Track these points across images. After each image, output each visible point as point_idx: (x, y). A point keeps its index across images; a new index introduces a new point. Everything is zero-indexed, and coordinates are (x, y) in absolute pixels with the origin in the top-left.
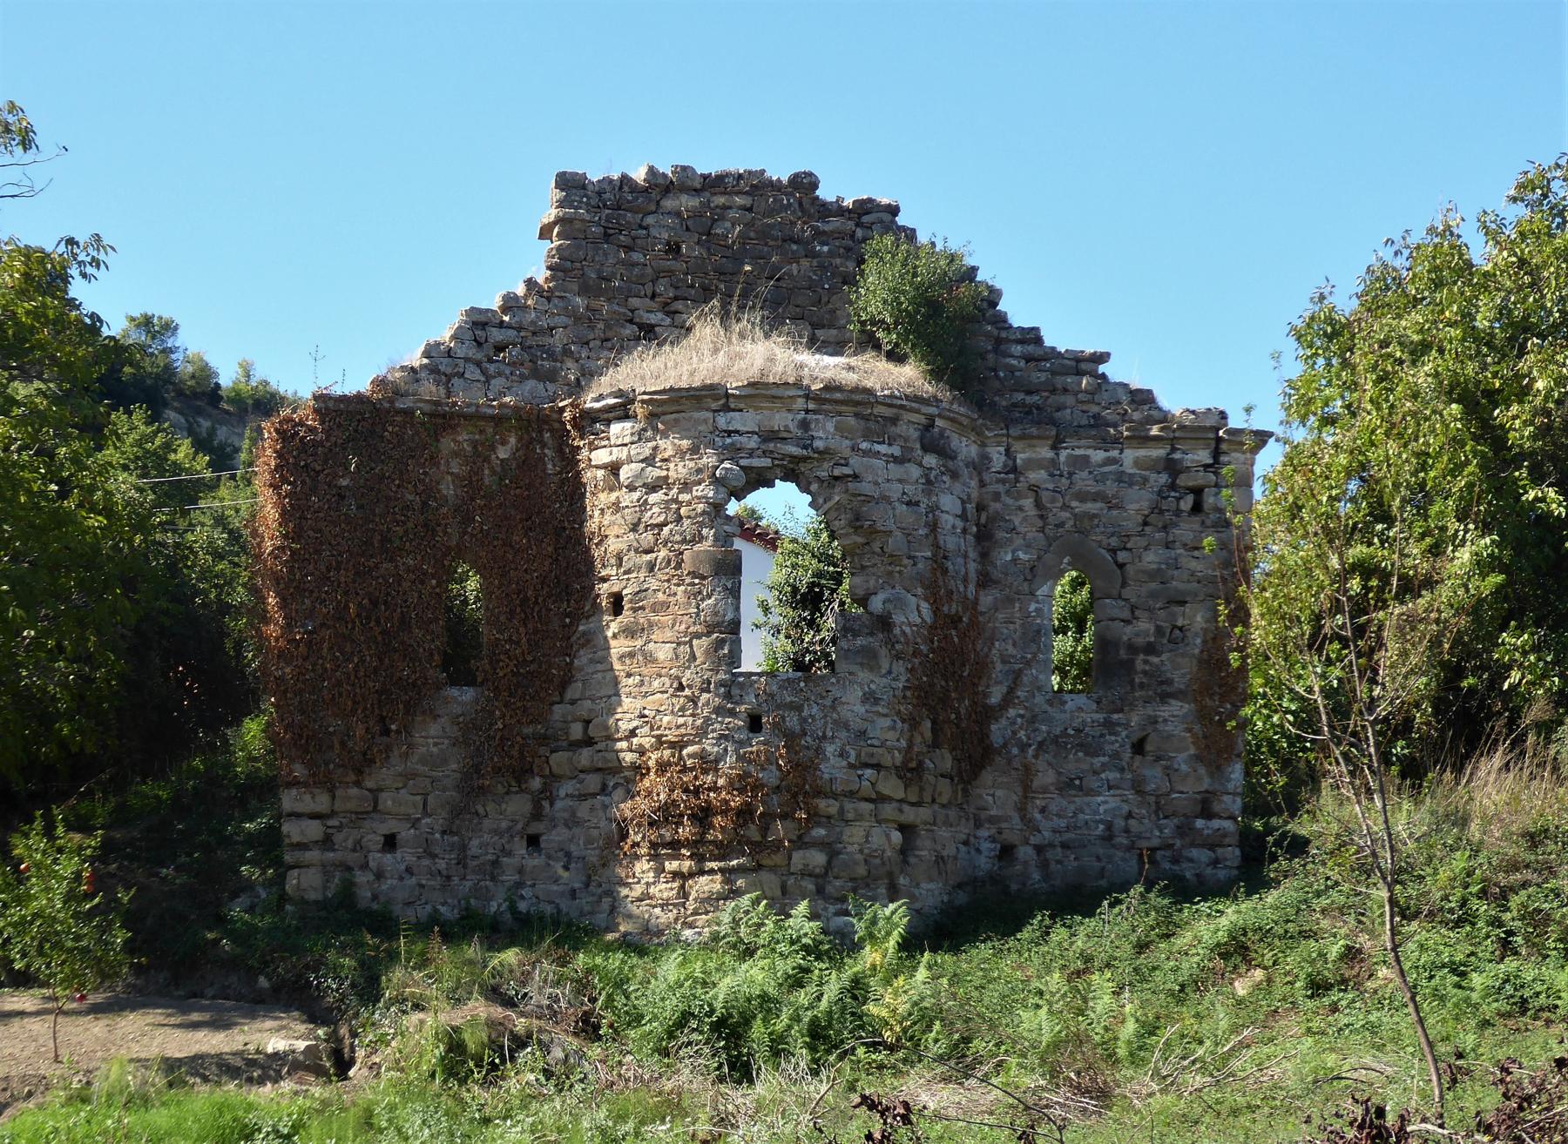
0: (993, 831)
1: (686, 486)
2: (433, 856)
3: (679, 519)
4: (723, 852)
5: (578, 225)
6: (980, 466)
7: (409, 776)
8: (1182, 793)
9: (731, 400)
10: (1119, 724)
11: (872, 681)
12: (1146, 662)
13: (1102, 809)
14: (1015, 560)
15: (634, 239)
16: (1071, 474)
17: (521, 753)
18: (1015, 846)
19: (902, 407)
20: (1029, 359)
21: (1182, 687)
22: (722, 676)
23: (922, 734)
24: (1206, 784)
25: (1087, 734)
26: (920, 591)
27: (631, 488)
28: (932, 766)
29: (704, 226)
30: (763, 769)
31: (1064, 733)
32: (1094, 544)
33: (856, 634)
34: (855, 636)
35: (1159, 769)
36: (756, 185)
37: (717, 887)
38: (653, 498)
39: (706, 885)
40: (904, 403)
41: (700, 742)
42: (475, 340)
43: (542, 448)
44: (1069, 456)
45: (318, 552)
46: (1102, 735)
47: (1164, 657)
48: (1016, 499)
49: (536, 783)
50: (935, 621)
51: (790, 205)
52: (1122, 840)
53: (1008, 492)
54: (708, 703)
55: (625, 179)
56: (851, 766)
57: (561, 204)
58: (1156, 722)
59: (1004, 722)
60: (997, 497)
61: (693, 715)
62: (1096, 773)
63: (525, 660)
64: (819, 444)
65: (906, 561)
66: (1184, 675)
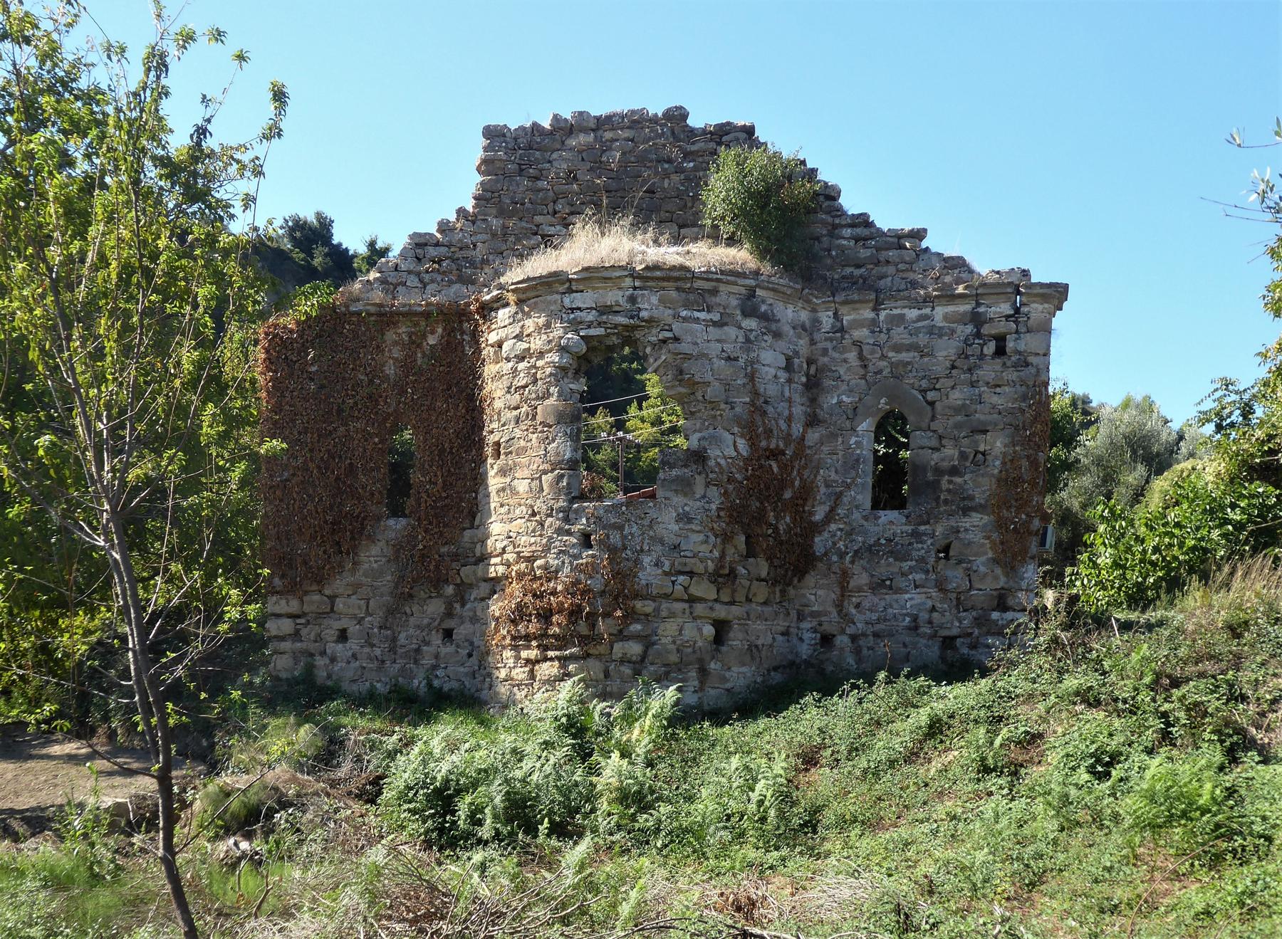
0: (814, 624)
1: (541, 355)
2: (372, 646)
3: (535, 381)
4: (562, 642)
5: (498, 164)
6: (809, 329)
7: (356, 587)
8: (980, 590)
9: (573, 283)
10: (925, 534)
11: (686, 505)
13: (908, 605)
14: (840, 403)
15: (541, 171)
16: (888, 330)
17: (437, 567)
18: (834, 636)
19: (718, 280)
21: (982, 502)
22: (561, 504)
23: (736, 547)
24: (1002, 582)
25: (897, 544)
26: (736, 430)
27: (508, 359)
28: (744, 571)
30: (591, 577)
31: (877, 542)
33: (672, 467)
35: (961, 571)
36: (637, 121)
37: (555, 671)
38: (521, 366)
39: (548, 669)
40: (719, 276)
41: (545, 557)
42: (417, 257)
43: (462, 334)
44: (888, 316)
45: (293, 421)
46: (910, 544)
47: (967, 477)
49: (450, 590)
50: (752, 453)
51: (663, 133)
52: (926, 630)
53: (834, 348)
54: (551, 526)
56: (666, 574)
57: (486, 149)
58: (958, 532)
59: (826, 535)
60: (825, 352)
61: (541, 535)
62: (903, 574)
63: (440, 497)
64: (644, 314)
65: (723, 406)
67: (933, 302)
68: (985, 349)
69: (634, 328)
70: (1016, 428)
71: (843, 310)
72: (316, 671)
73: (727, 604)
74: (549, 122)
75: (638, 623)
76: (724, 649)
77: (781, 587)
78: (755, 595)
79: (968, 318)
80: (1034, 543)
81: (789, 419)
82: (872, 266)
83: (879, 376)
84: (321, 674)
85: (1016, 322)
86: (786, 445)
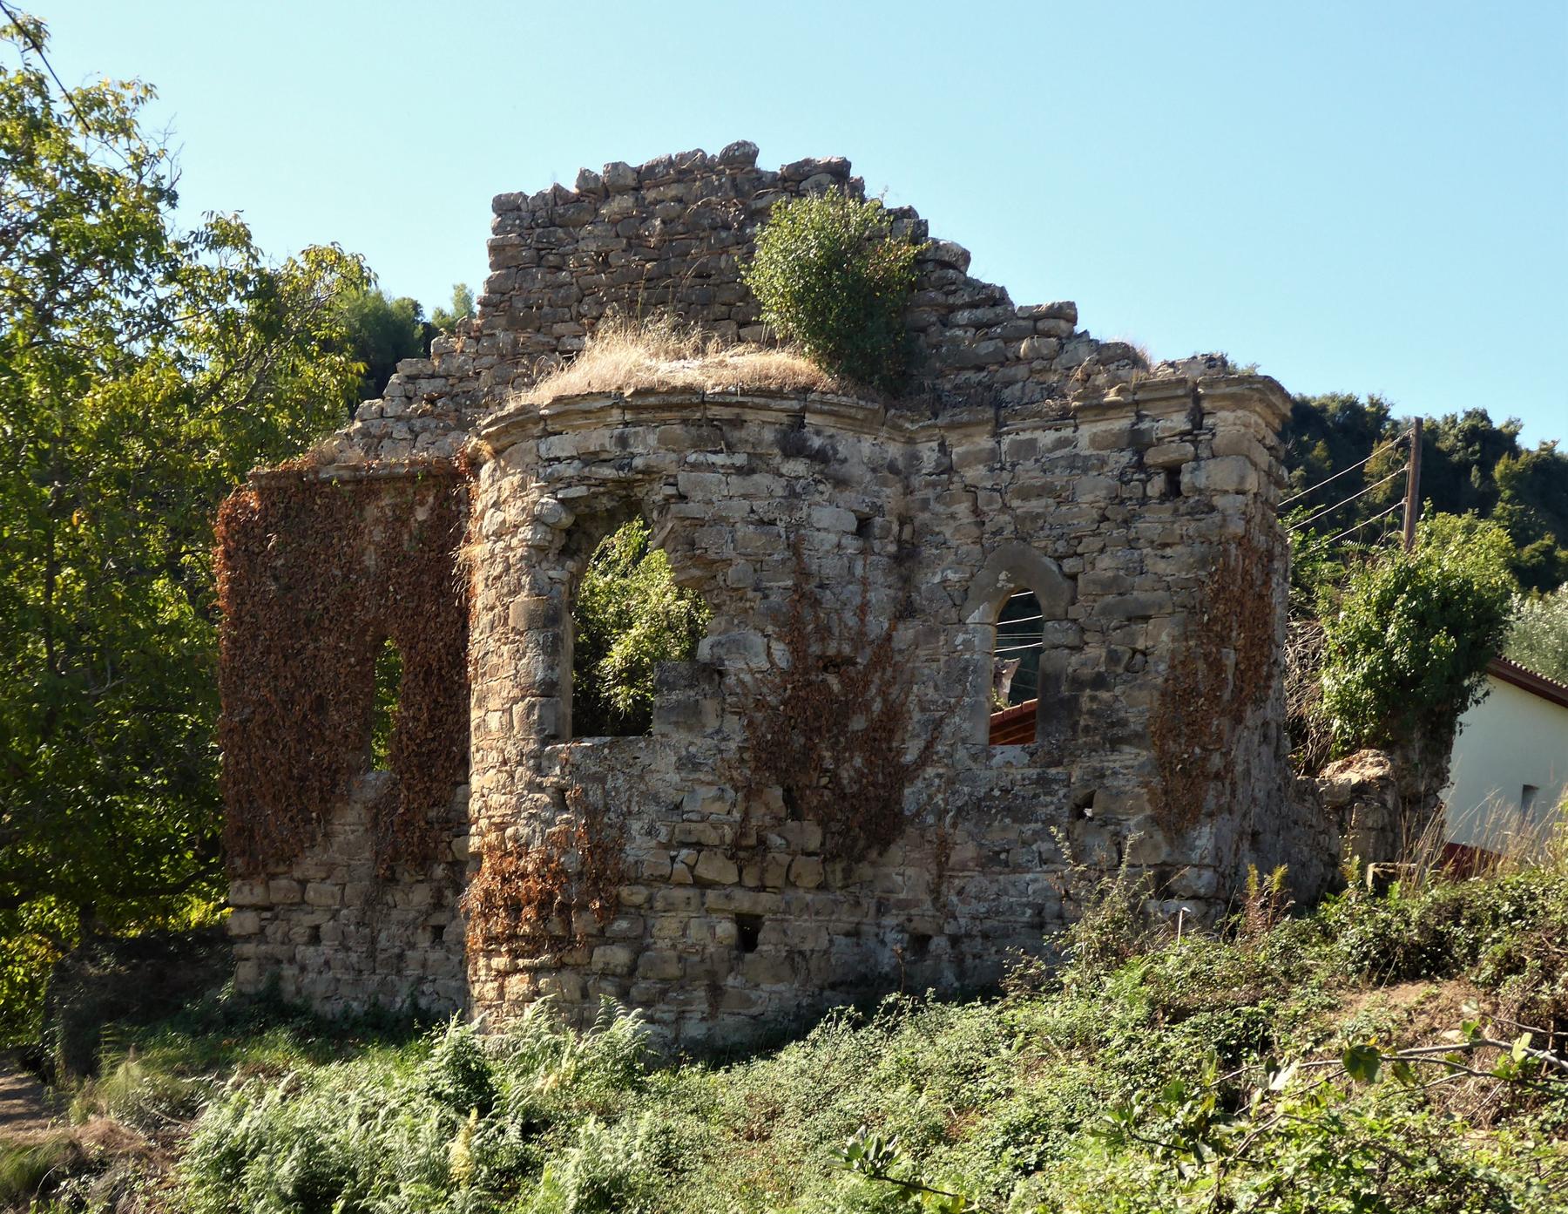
0: (902, 918)
4: (534, 945)
5: (510, 252)
9: (549, 422)
10: (1055, 781)
11: (691, 744)
12: (1093, 699)
14: (945, 580)
16: (1014, 465)
17: (422, 838)
20: (978, 325)
21: (1139, 728)
22: (533, 746)
23: (767, 805)
24: (1163, 854)
25: (1016, 796)
26: (770, 629)
28: (779, 841)
29: (629, 232)
30: (565, 852)
31: (989, 795)
32: (1037, 553)
34: (670, 690)
35: (1107, 836)
39: (517, 985)
44: (1013, 442)
46: (1036, 796)
47: (1118, 690)
48: (948, 505)
49: (439, 871)
53: (938, 498)
55: (557, 189)
57: (495, 230)
58: (1103, 776)
59: (919, 784)
60: (925, 504)
62: (1025, 843)
65: (750, 594)
66: (1142, 713)
67: (1074, 417)
68: (1149, 487)
69: (628, 484)
70: (1192, 611)
71: (951, 438)
72: (282, 984)
73: (751, 889)
74: (574, 183)
75: (623, 919)
76: (749, 956)
77: (844, 864)
78: (799, 876)
79: (1124, 441)
80: (1211, 792)
81: (863, 609)
82: (995, 367)
83: (998, 538)
84: (289, 988)
85: (1195, 443)
86: (855, 649)
